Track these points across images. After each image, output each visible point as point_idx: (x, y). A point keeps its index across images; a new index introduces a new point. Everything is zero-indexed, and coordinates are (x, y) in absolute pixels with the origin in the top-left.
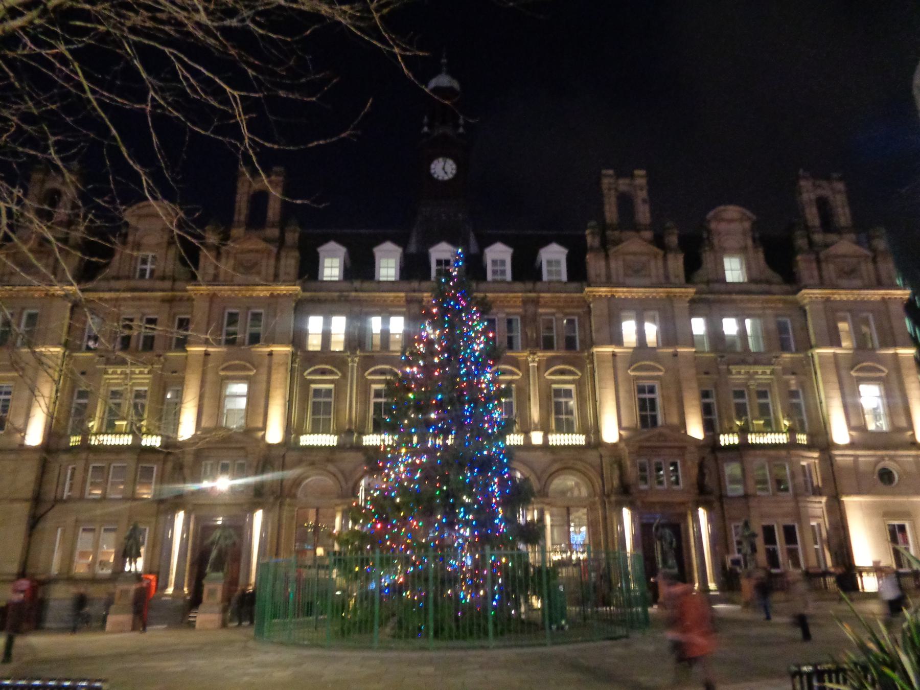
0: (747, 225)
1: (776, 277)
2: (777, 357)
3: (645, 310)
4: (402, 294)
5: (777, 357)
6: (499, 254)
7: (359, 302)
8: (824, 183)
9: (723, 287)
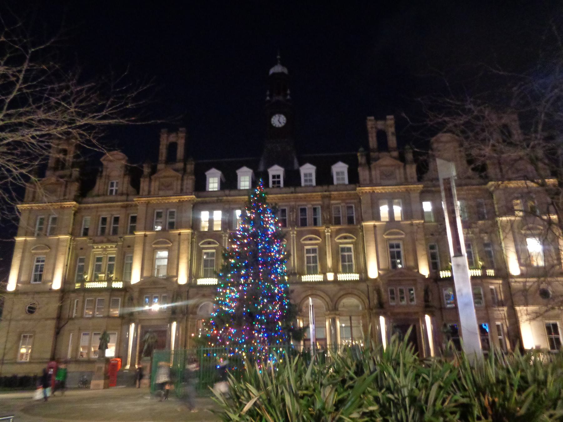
6: (308, 170)
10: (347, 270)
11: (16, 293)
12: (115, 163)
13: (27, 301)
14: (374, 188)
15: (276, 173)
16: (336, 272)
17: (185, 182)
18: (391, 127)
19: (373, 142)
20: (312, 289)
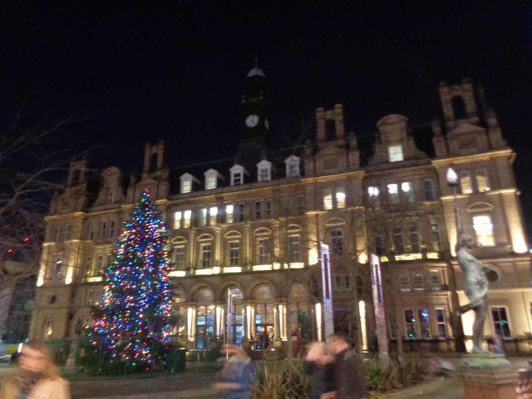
0: (403, 124)
1: (422, 154)
2: (420, 205)
3: (336, 187)
4: (213, 196)
5: (420, 205)
6: (264, 166)
7: (194, 202)
8: (457, 87)
9: (387, 166)
10: (234, 263)
11: (42, 287)
12: (112, 176)
13: (51, 293)
14: (316, 178)
15: (237, 172)
16: (223, 266)
17: (160, 187)
18: (339, 115)
19: (448, 111)
20: (260, 278)
